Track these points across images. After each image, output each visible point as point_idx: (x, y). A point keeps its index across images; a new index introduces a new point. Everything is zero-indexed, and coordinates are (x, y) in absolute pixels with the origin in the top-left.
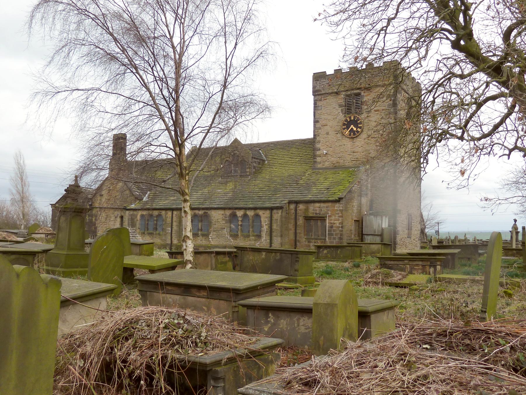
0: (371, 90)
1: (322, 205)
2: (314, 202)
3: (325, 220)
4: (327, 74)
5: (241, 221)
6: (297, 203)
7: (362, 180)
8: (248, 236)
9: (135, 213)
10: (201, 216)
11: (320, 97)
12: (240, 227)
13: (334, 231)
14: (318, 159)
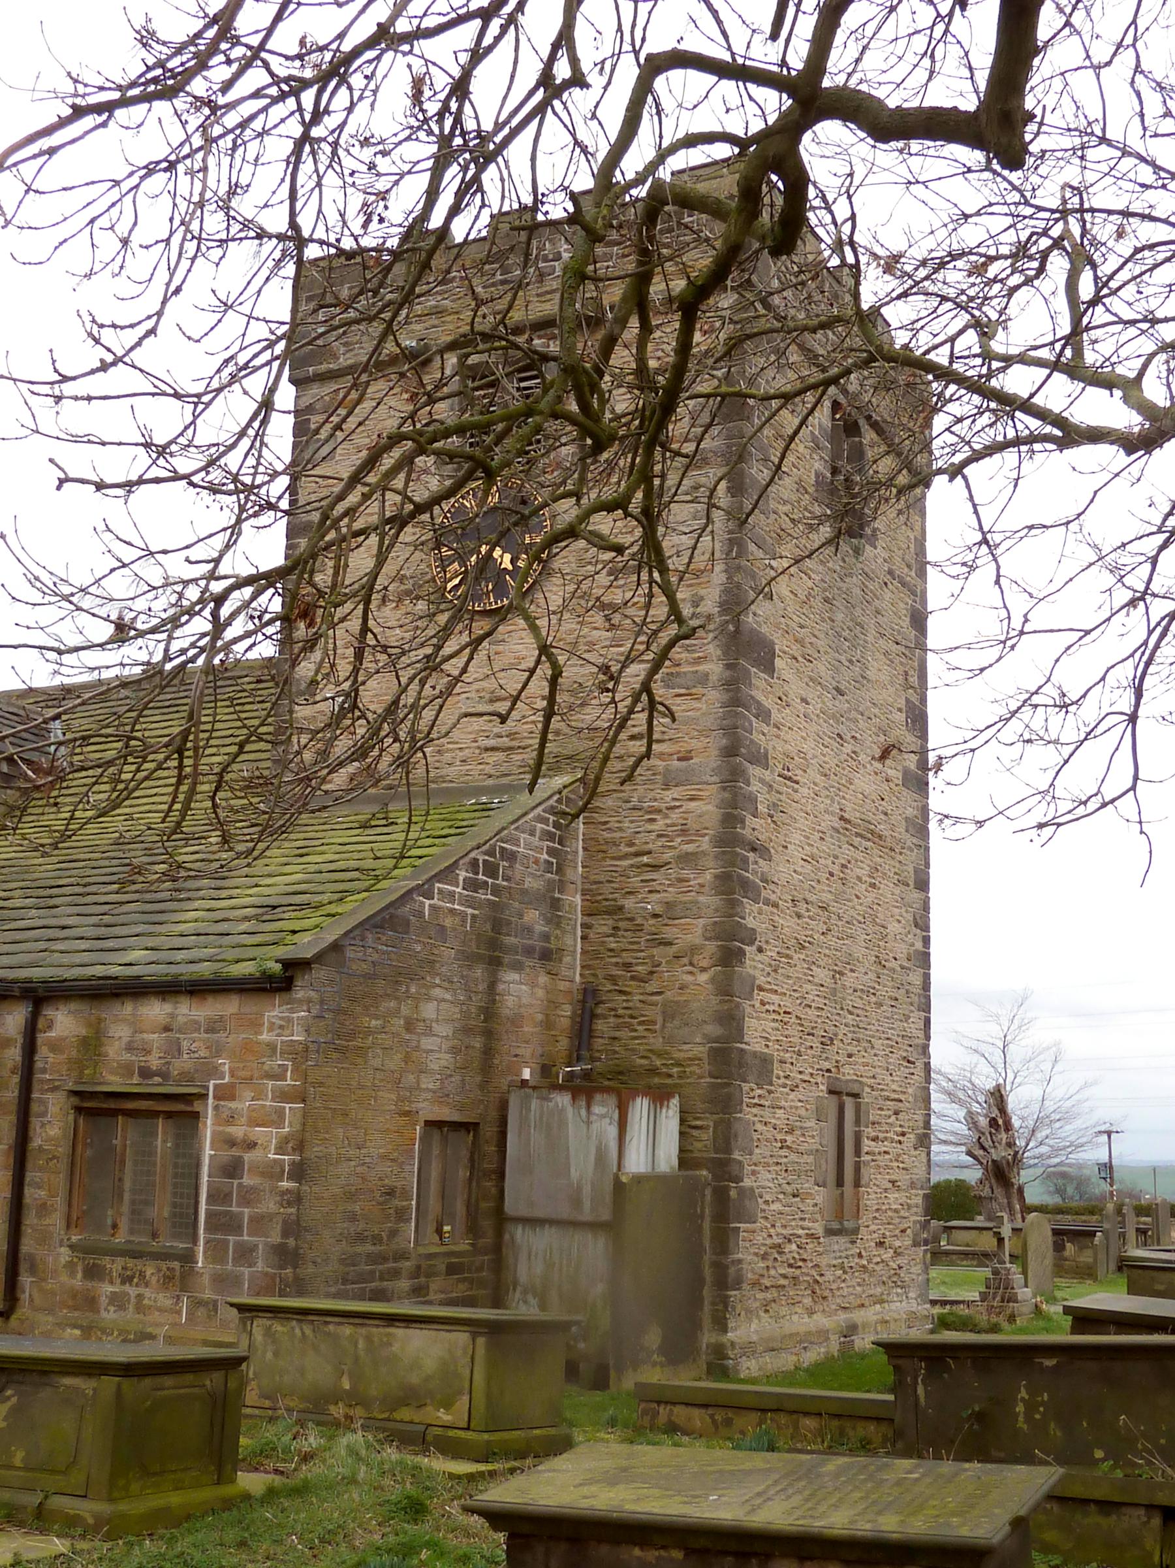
1: (186, 1010)
3: (196, 1116)
7: (511, 857)
13: (248, 1197)
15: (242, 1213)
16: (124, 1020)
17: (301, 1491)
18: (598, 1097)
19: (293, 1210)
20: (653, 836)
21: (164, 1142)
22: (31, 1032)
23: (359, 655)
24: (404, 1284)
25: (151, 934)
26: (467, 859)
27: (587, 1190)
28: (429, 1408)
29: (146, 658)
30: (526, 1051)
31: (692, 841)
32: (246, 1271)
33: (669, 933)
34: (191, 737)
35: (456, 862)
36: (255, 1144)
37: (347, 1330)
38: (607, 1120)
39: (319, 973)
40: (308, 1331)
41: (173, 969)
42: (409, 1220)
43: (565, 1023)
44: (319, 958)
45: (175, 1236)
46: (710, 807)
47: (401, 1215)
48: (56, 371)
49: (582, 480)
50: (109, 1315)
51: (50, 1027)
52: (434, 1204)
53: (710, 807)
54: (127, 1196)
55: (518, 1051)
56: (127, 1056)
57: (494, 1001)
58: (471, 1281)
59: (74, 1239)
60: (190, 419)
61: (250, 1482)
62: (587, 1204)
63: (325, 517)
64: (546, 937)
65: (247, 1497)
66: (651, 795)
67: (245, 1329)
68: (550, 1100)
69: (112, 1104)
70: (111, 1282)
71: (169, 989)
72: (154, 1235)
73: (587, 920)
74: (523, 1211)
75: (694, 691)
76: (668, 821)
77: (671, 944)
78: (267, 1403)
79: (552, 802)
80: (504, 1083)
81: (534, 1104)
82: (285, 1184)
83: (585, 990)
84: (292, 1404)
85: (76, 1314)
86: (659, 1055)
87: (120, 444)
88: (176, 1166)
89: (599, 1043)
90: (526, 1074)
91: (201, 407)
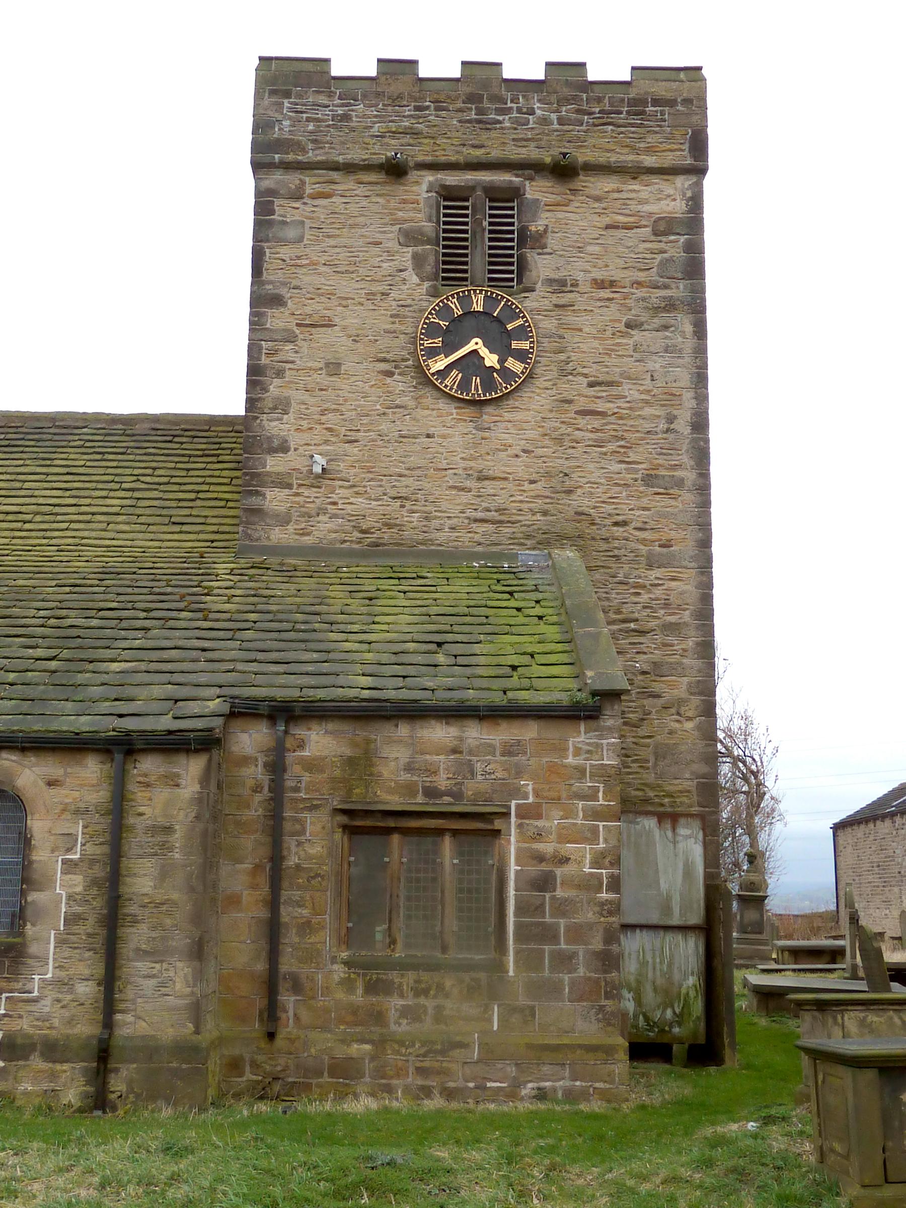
0: (577, 184)
1: (474, 733)
2: (413, 712)
4: (335, 72)
6: (285, 713)
11: (292, 179)
13: (562, 908)
14: (275, 499)
15: (558, 924)
16: (400, 742)
18: (682, 821)
20: (639, 607)
31: (674, 614)
32: (566, 978)
33: (657, 687)
36: (568, 859)
38: (693, 840)
46: (688, 587)
51: (301, 745)
53: (688, 587)
56: (405, 777)
62: (676, 910)
66: (636, 573)
68: (638, 823)
69: (391, 823)
70: (402, 996)
72: (444, 949)
75: (671, 491)
76: (653, 596)
77: (659, 696)
82: (604, 895)
85: (358, 1029)
86: (652, 787)
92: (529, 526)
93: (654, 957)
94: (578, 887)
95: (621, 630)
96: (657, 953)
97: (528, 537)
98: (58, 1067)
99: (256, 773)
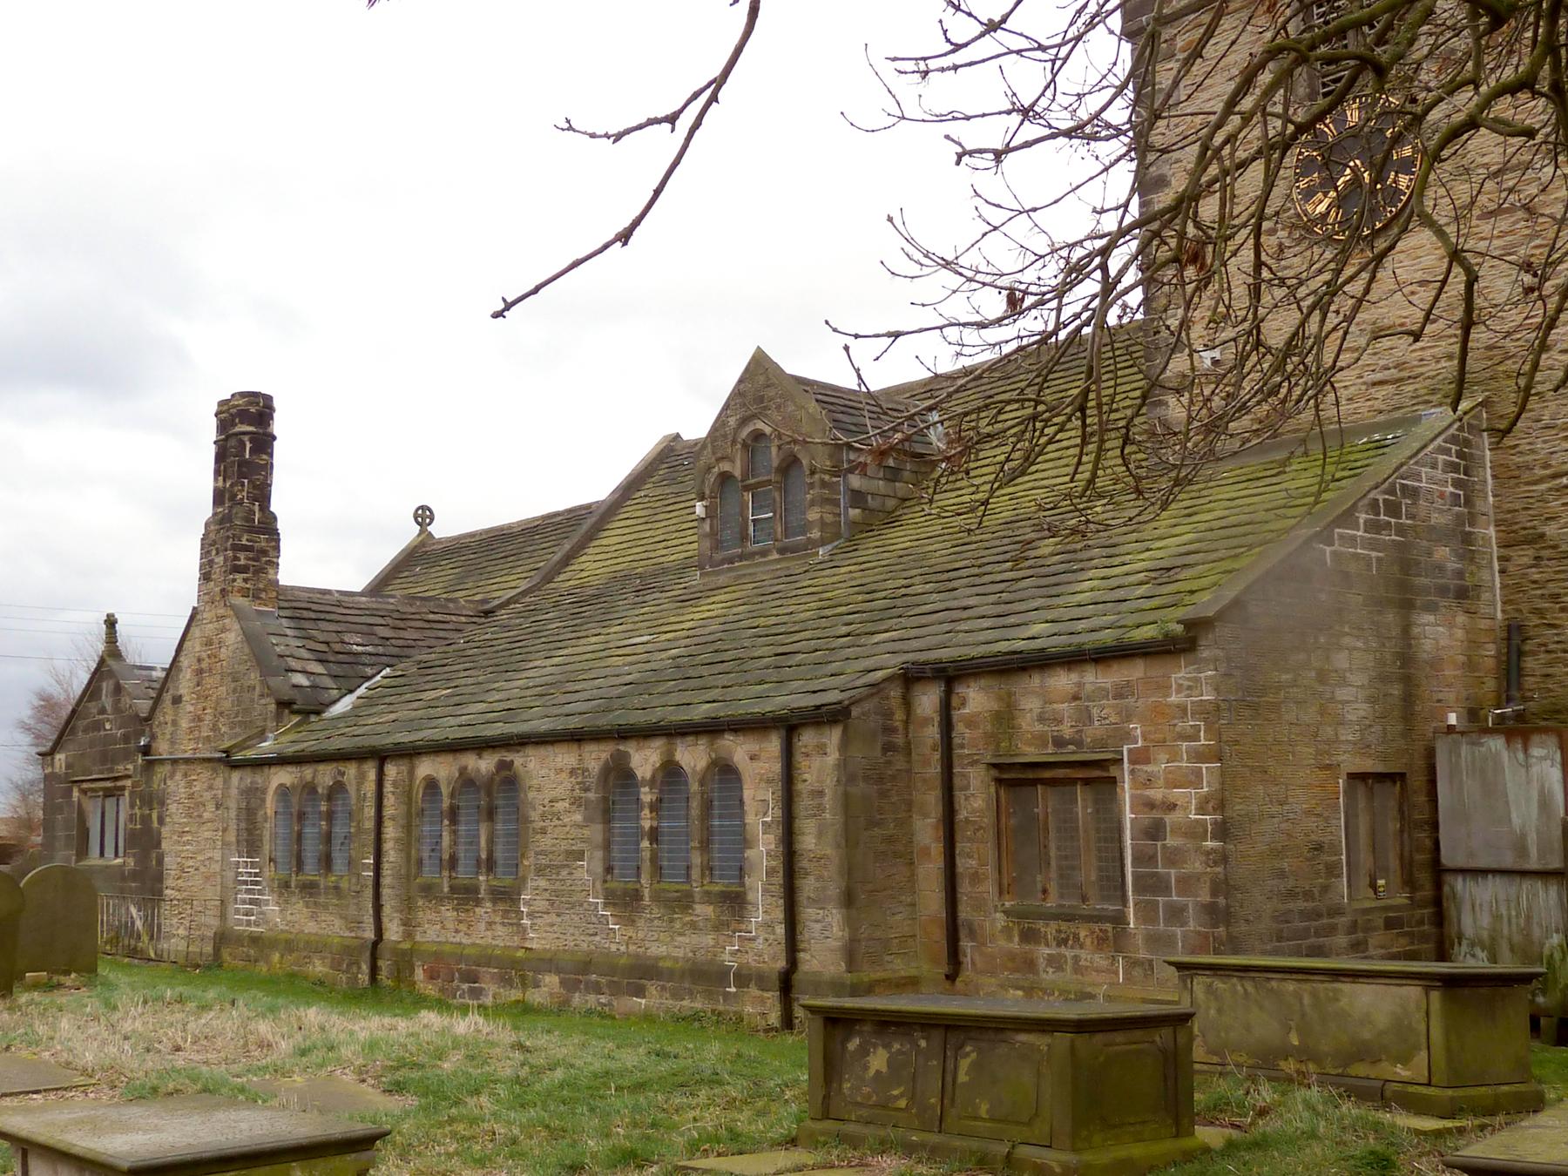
1: (1092, 678)
2: (1041, 662)
3: (1113, 781)
5: (655, 807)
6: (951, 675)
7: (1413, 493)
8: (684, 902)
9: (258, 778)
10: (488, 785)
12: (645, 844)
13: (1173, 858)
17: (1261, 1144)
18: (1536, 738)
19: (1219, 869)
21: (1085, 808)
22: (946, 709)
23: (1255, 293)
24: (1342, 940)
25: (1049, 607)
26: (1365, 501)
27: (1532, 839)
28: (1384, 1064)
29: (1042, 328)
30: (1450, 696)
32: (1179, 931)
34: (1092, 396)
35: (1355, 504)
37: (1291, 987)
39: (1223, 631)
40: (1250, 989)
41: (1076, 639)
42: (1340, 876)
43: (1490, 663)
44: (1221, 615)
45: (1105, 899)
47: (1332, 870)
48: (948, 40)
49: (1479, 66)
50: (1048, 976)
51: (964, 704)
52: (1365, 859)
54: (1053, 863)
55: (1440, 696)
56: (1039, 727)
57: (1410, 646)
58: (1410, 935)
59: (1007, 904)
60: (1049, 77)
61: (1209, 1135)
62: (1533, 851)
63: (1205, 148)
64: (1460, 574)
65: (1207, 1150)
67: (1185, 986)
68: (1482, 745)
69: (1030, 775)
71: (1074, 659)
72: (1084, 899)
73: (1504, 552)
74: (1460, 861)
78: (1215, 1059)
79: (1452, 431)
80: (1429, 729)
81: (1465, 750)
82: (1209, 844)
83: (1509, 626)
84: (1241, 1060)
85: (1017, 975)
87: (984, 115)
88: (1098, 830)
89: (1529, 682)
90: (1452, 719)
91: (1058, 63)
92: (1433, 378)
93: (1509, 909)
94: (1186, 835)
95: (1550, 489)
96: (1513, 905)
97: (1433, 391)
98: (766, 995)
99: (933, 733)
